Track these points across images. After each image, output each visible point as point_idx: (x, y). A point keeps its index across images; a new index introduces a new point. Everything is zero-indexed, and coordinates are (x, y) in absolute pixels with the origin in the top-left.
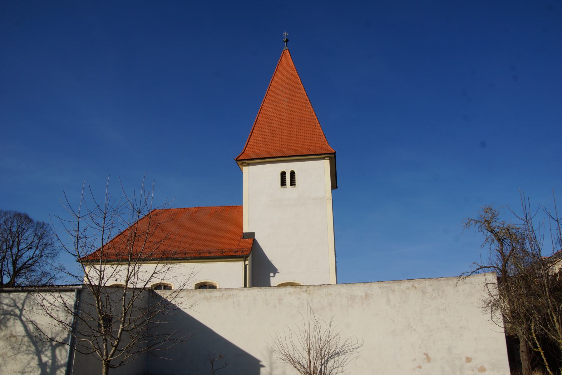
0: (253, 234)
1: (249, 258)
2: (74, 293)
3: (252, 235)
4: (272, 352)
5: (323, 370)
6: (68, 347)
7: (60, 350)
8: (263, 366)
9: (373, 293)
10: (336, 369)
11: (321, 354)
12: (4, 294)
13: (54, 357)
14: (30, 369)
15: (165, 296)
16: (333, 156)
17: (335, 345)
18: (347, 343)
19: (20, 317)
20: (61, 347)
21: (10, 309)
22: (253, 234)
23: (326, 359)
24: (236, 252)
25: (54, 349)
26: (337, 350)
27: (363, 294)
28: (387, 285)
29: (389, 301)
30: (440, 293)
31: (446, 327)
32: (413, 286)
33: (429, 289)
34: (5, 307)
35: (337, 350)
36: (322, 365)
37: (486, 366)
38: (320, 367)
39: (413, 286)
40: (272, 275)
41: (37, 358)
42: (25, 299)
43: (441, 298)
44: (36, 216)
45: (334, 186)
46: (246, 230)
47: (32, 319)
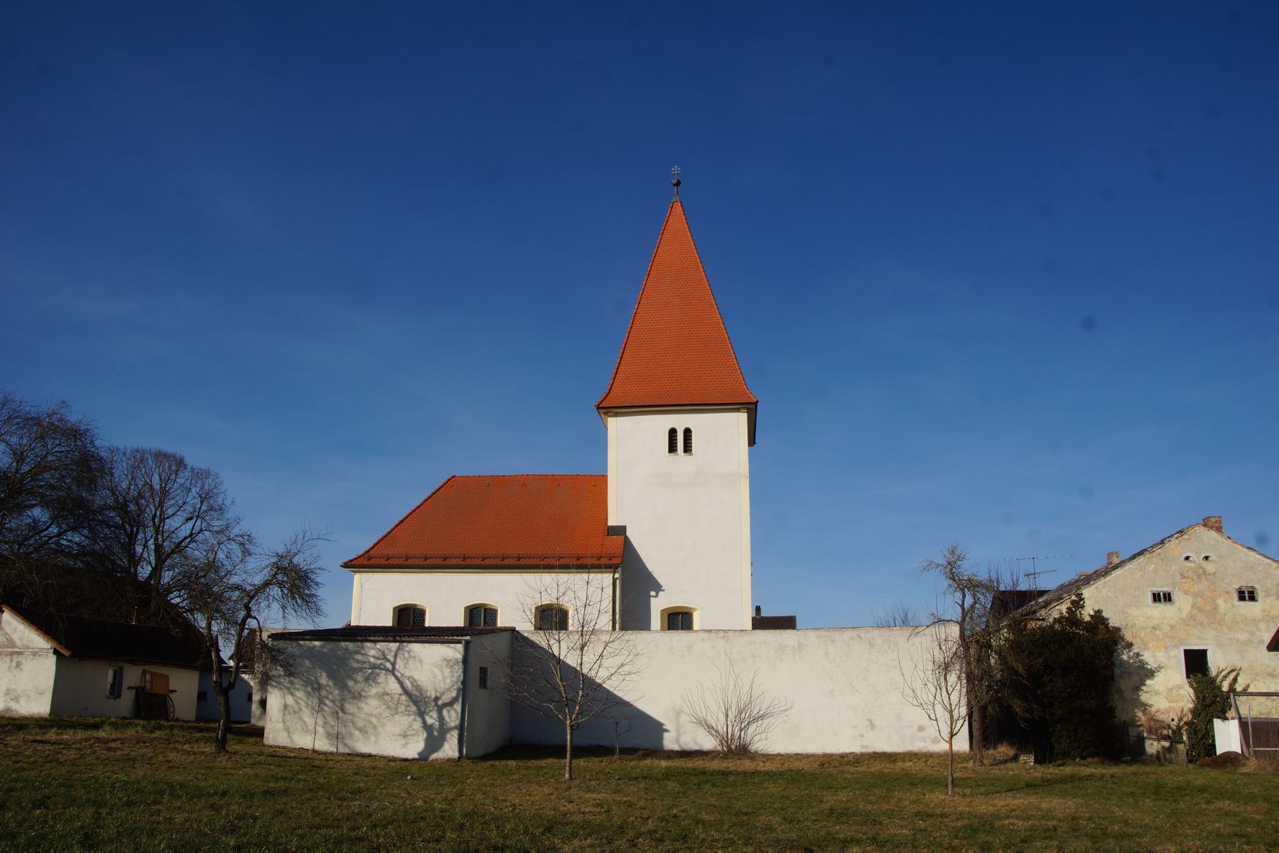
0: (624, 528)
3: (621, 530)
4: (678, 713)
6: (458, 707)
8: (667, 731)
12: (368, 644)
13: (441, 718)
15: (544, 644)
17: (759, 706)
19: (393, 672)
22: (624, 528)
25: (440, 709)
29: (827, 654)
33: (878, 641)
34: (372, 660)
40: (653, 593)
44: (195, 458)
45: (752, 441)
46: (612, 522)
47: (408, 674)
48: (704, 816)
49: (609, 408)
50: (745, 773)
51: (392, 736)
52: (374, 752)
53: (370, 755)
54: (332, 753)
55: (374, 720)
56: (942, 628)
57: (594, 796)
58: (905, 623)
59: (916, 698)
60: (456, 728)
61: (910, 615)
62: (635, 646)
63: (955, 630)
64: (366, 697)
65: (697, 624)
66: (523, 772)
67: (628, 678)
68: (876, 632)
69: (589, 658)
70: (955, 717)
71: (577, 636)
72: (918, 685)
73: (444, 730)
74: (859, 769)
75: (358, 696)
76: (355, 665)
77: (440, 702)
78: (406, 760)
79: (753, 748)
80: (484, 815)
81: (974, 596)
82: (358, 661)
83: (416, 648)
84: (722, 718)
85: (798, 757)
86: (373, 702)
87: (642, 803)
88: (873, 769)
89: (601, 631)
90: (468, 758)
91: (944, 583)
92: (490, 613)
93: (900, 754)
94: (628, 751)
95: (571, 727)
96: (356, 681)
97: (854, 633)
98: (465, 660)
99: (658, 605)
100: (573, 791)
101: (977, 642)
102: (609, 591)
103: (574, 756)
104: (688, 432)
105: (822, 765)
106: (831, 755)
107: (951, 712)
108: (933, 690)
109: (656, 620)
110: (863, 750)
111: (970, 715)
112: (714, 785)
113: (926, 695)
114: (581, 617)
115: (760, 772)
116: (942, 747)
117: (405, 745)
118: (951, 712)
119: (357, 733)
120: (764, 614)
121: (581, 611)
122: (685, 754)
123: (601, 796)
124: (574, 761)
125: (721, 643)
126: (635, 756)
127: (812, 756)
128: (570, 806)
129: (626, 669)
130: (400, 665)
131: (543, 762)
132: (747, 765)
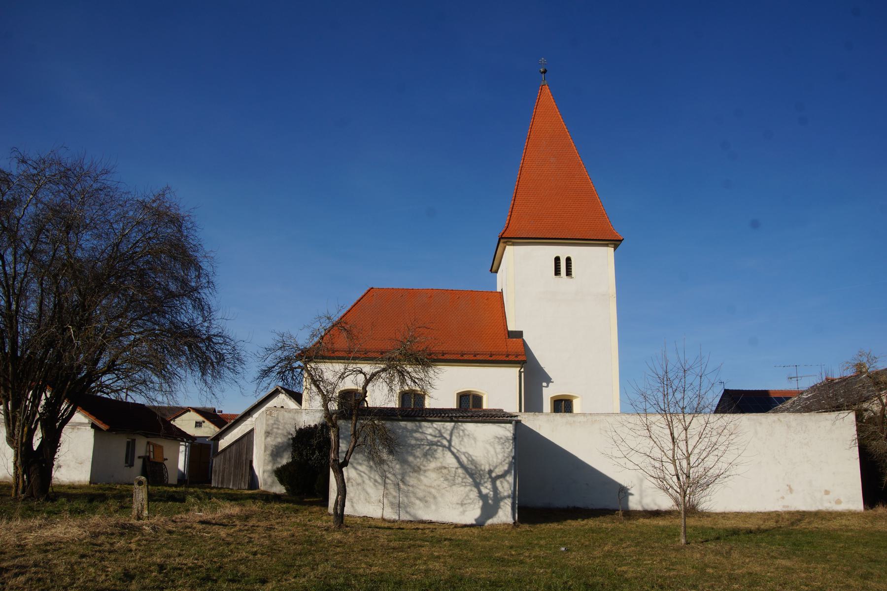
3: (519, 334)
6: (510, 478)
7: (501, 482)
12: (425, 424)
13: (495, 489)
14: (470, 501)
21: (436, 439)
24: (508, 356)
34: (429, 437)
37: (842, 499)
40: (544, 384)
41: (476, 490)
42: (452, 430)
46: (511, 328)
47: (463, 450)
49: (507, 239)
51: (450, 504)
52: (434, 520)
53: (431, 522)
54: (394, 521)
55: (433, 491)
60: (509, 497)
64: (425, 471)
73: (498, 498)
75: (417, 470)
76: (413, 442)
77: (494, 475)
78: (465, 526)
79: (700, 507)
82: (416, 439)
83: (470, 427)
86: (433, 475)
92: (477, 399)
96: (415, 457)
98: (515, 438)
99: (549, 393)
104: (568, 260)
109: (547, 406)
117: (464, 512)
119: (418, 502)
130: (455, 442)
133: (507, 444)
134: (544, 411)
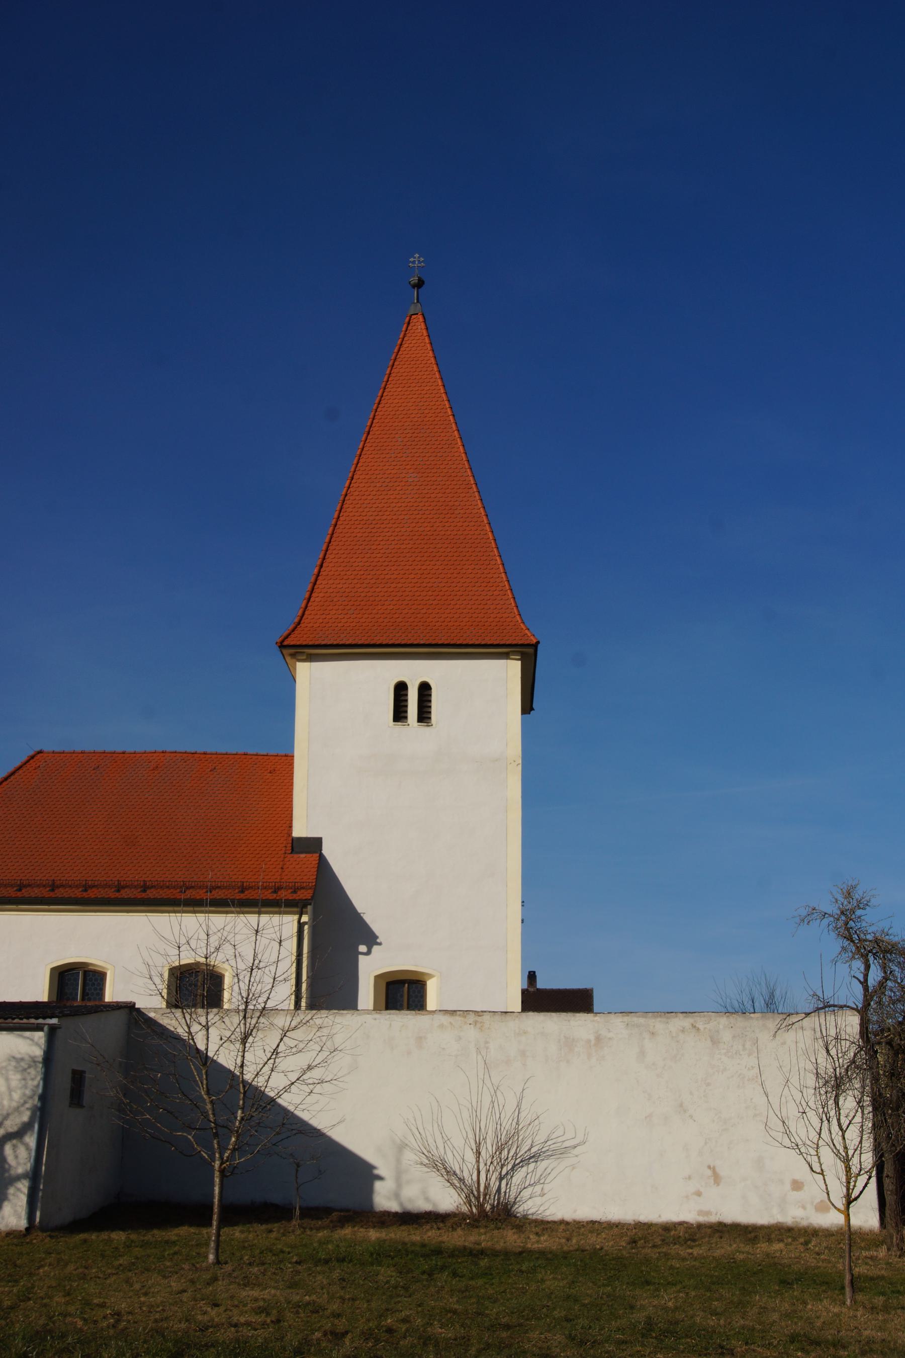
1: (310, 908)
2: (41, 1034)
3: (314, 845)
4: (402, 1147)
5: (503, 1190)
6: (31, 1140)
7: (15, 1147)
8: (380, 1178)
9: (610, 1035)
10: (530, 1189)
11: (501, 1159)
15: (181, 1031)
16: (531, 650)
18: (554, 1136)
20: (14, 1141)
23: (510, 1167)
24: (276, 890)
26: (533, 1150)
27: (592, 1037)
28: (642, 1020)
29: (642, 1053)
30: (748, 1045)
31: (755, 1115)
32: (694, 1026)
33: (726, 1036)
35: (533, 1150)
36: (501, 1179)
38: (497, 1183)
39: (694, 1026)
40: (363, 948)
43: (749, 1055)
45: (527, 706)
46: (300, 830)
48: (437, 1330)
50: (506, 1254)
56: (831, 1018)
57: (255, 1293)
58: (770, 1006)
59: (787, 1133)
60: (24, 1176)
61: (777, 993)
62: (330, 1037)
63: (851, 1023)
65: (432, 1001)
66: (137, 1251)
67: (318, 1089)
68: (723, 1021)
69: (256, 1055)
70: (855, 1170)
71: (236, 1019)
72: (792, 1111)
74: (696, 1251)
80: (63, 1336)
81: (884, 968)
84: (470, 1157)
85: (594, 1226)
87: (335, 1307)
88: (718, 1253)
89: (275, 1010)
90: (43, 1228)
91: (834, 944)
93: (762, 1228)
94: (313, 1213)
95: (222, 1172)
97: (686, 1022)
98: (48, 1059)
100: (221, 1285)
101: (889, 1043)
102: (291, 945)
103: (224, 1221)
105: (634, 1242)
106: (648, 1226)
107: (847, 1161)
108: (816, 1122)
109: (366, 994)
110: (702, 1219)
111: (879, 1166)
112: (455, 1274)
113: (804, 1131)
114: (244, 987)
115: (530, 1252)
116: (833, 1219)
118: (847, 1161)
120: (541, 984)
121: (245, 976)
122: (409, 1218)
123: (266, 1294)
124: (225, 1230)
125: (471, 1033)
126: (326, 1221)
127: (618, 1225)
128: (213, 1312)
129: (316, 1074)
131: (173, 1234)
132: (510, 1239)
133: (32, 1071)
134: (361, 1006)
